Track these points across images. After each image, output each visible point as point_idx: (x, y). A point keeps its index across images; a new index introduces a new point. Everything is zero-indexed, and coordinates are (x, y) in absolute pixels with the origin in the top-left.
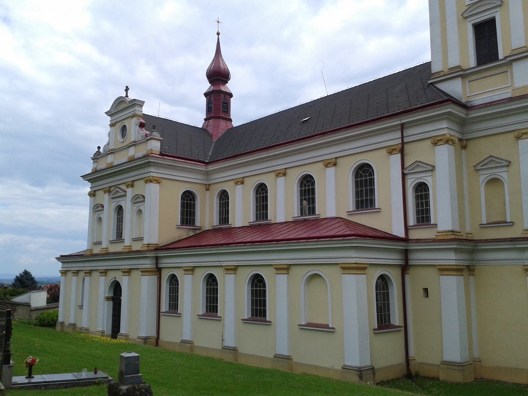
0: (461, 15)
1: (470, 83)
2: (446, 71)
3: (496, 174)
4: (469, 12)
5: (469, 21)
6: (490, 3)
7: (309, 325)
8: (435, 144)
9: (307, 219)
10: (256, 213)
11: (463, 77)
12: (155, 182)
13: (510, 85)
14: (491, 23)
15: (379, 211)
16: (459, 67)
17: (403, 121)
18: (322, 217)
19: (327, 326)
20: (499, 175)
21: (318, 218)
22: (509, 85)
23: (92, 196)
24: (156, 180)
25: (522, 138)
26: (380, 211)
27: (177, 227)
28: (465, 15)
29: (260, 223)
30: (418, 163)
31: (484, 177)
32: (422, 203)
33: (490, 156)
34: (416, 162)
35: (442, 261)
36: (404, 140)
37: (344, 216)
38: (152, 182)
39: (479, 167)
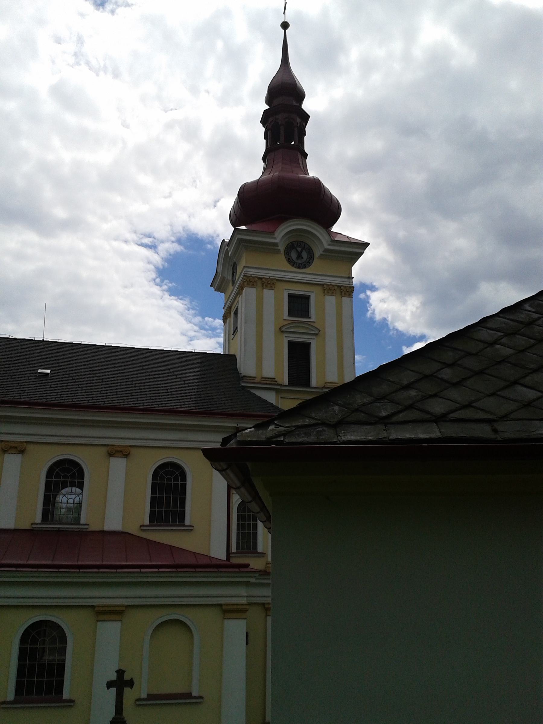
0: (320, 331)
2: (258, 380)
4: (287, 328)
5: (285, 337)
7: (150, 697)
8: (111, 455)
9: (60, 529)
10: (237, 514)
14: (306, 347)
15: (190, 529)
16: (272, 379)
18: (94, 527)
19: (188, 695)
20: (62, 499)
21: (85, 530)
28: (283, 329)
29: (59, 528)
32: (249, 525)
35: (41, 600)
37: (134, 529)
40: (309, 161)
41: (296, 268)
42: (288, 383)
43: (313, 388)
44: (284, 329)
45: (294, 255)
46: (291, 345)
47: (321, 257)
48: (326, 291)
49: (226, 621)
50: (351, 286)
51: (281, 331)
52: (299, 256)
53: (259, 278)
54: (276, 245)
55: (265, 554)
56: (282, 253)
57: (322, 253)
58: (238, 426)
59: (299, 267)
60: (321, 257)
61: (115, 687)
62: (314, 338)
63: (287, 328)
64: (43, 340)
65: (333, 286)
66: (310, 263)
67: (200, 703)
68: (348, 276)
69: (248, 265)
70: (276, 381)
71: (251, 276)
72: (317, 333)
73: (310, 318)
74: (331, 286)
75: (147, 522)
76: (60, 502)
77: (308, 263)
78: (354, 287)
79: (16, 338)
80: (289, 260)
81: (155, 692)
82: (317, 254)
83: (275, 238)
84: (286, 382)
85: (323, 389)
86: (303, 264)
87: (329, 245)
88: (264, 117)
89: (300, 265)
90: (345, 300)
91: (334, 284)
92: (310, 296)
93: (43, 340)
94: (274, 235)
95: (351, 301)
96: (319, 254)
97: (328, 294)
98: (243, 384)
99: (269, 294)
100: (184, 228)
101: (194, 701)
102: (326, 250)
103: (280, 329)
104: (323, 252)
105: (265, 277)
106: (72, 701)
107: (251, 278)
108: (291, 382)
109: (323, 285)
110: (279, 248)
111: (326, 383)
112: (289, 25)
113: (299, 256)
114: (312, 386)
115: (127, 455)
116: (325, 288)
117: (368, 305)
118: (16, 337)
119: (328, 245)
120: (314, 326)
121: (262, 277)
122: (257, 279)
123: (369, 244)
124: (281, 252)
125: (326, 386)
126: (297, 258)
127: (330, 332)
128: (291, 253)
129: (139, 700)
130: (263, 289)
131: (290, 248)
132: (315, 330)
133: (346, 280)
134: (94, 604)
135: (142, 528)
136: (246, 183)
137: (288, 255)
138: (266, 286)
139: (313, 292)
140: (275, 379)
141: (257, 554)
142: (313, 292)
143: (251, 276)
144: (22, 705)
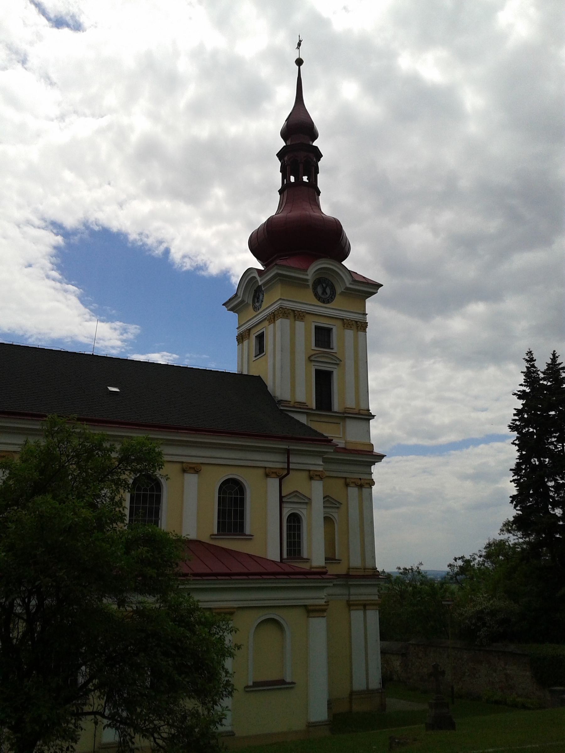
2: (292, 404)
4: (315, 358)
6: (332, 358)
7: (256, 684)
8: (184, 471)
12: (274, 475)
13: (341, 436)
14: (329, 375)
15: (250, 538)
17: (291, 447)
19: (282, 682)
22: (339, 436)
24: (194, 468)
26: (251, 539)
28: (312, 358)
30: (296, 493)
32: (294, 534)
36: (290, 466)
37: (205, 538)
38: (269, 475)
39: (306, 501)
40: (322, 199)
41: (321, 302)
43: (336, 412)
45: (320, 290)
46: (318, 372)
47: (342, 293)
49: (311, 620)
50: (365, 321)
51: (310, 359)
52: (324, 292)
53: (292, 310)
54: (307, 280)
55: (309, 559)
57: (343, 290)
58: (289, 448)
59: (324, 302)
60: (342, 293)
62: (336, 367)
64: (93, 354)
67: (292, 688)
68: (362, 312)
69: (282, 298)
70: (307, 406)
71: (301, 311)
72: (338, 362)
73: (332, 349)
74: (350, 321)
75: (216, 532)
78: (367, 323)
79: (68, 351)
80: (316, 295)
81: (260, 679)
82: (339, 290)
83: (307, 275)
84: (314, 407)
85: (344, 414)
86: (327, 299)
87: (350, 284)
88: (283, 150)
89: (325, 300)
90: (361, 333)
91: (352, 319)
92: (332, 328)
93: (93, 354)
94: (307, 272)
95: (366, 334)
96: (340, 291)
98: (282, 408)
99: (300, 325)
100: (96, 219)
101: (288, 686)
102: (347, 289)
103: (309, 358)
104: (344, 289)
105: (298, 310)
106: (293, 683)
109: (343, 319)
111: (360, 410)
112: (303, 61)
113: (324, 292)
114: (335, 410)
115: (198, 471)
116: (358, 324)
117: (59, 261)
118: (68, 350)
120: (335, 356)
121: (295, 309)
122: (290, 311)
123: (382, 285)
124: (309, 287)
125: (346, 411)
126: (323, 294)
127: (349, 363)
128: (317, 288)
129: (247, 687)
131: (318, 282)
132: (337, 360)
133: (361, 316)
134: (210, 607)
135: (213, 537)
136: (269, 219)
137: (315, 290)
138: (298, 318)
139: (335, 325)
140: (305, 403)
141: (303, 560)
142: (335, 325)
144: (279, 687)
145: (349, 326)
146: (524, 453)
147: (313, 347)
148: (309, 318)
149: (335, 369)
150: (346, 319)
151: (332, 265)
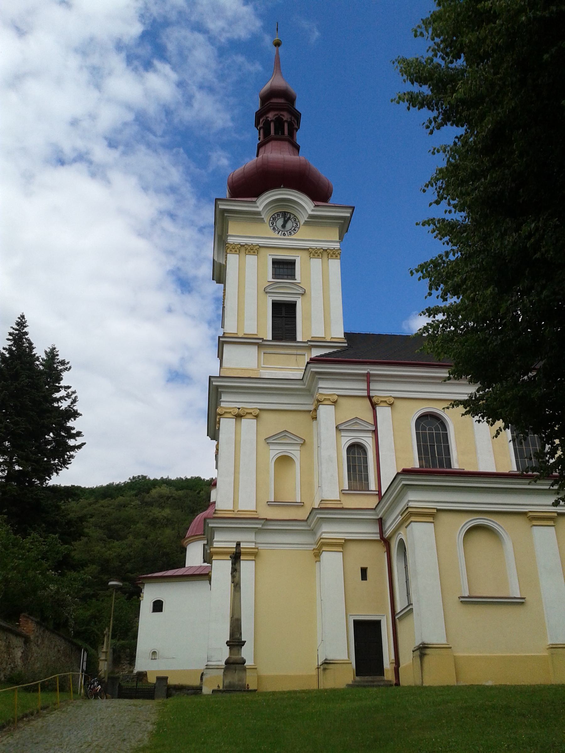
1: (265, 354)
3: (361, 438)
4: (270, 289)
5: (269, 296)
11: (259, 345)
14: (292, 306)
23: (421, 27)
25: (246, 417)
27: (461, 601)
28: (268, 290)
31: (274, 452)
33: (285, 430)
34: (355, 419)
39: (270, 441)
42: (272, 338)
44: (268, 289)
46: (277, 306)
47: (307, 223)
48: (312, 255)
54: (259, 213)
56: (266, 222)
60: (307, 223)
61: (558, 439)
63: (270, 289)
65: (319, 249)
66: (295, 230)
71: (234, 244)
76: (245, 422)
77: (294, 231)
83: (258, 207)
85: (308, 343)
87: (313, 210)
94: (256, 203)
96: (304, 221)
97: (217, 212)
99: (251, 260)
102: (311, 217)
107: (234, 245)
108: (275, 337)
109: (308, 249)
110: (263, 217)
119: (312, 211)
130: (329, 259)
135: (343, 492)
143: (234, 244)
145: (316, 255)
146: (542, 428)
147: (271, 279)
148: (263, 252)
149: (298, 299)
150: (311, 248)
151: (280, 194)
